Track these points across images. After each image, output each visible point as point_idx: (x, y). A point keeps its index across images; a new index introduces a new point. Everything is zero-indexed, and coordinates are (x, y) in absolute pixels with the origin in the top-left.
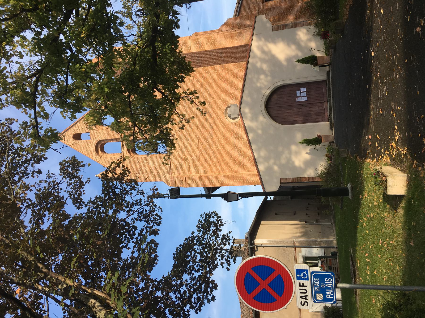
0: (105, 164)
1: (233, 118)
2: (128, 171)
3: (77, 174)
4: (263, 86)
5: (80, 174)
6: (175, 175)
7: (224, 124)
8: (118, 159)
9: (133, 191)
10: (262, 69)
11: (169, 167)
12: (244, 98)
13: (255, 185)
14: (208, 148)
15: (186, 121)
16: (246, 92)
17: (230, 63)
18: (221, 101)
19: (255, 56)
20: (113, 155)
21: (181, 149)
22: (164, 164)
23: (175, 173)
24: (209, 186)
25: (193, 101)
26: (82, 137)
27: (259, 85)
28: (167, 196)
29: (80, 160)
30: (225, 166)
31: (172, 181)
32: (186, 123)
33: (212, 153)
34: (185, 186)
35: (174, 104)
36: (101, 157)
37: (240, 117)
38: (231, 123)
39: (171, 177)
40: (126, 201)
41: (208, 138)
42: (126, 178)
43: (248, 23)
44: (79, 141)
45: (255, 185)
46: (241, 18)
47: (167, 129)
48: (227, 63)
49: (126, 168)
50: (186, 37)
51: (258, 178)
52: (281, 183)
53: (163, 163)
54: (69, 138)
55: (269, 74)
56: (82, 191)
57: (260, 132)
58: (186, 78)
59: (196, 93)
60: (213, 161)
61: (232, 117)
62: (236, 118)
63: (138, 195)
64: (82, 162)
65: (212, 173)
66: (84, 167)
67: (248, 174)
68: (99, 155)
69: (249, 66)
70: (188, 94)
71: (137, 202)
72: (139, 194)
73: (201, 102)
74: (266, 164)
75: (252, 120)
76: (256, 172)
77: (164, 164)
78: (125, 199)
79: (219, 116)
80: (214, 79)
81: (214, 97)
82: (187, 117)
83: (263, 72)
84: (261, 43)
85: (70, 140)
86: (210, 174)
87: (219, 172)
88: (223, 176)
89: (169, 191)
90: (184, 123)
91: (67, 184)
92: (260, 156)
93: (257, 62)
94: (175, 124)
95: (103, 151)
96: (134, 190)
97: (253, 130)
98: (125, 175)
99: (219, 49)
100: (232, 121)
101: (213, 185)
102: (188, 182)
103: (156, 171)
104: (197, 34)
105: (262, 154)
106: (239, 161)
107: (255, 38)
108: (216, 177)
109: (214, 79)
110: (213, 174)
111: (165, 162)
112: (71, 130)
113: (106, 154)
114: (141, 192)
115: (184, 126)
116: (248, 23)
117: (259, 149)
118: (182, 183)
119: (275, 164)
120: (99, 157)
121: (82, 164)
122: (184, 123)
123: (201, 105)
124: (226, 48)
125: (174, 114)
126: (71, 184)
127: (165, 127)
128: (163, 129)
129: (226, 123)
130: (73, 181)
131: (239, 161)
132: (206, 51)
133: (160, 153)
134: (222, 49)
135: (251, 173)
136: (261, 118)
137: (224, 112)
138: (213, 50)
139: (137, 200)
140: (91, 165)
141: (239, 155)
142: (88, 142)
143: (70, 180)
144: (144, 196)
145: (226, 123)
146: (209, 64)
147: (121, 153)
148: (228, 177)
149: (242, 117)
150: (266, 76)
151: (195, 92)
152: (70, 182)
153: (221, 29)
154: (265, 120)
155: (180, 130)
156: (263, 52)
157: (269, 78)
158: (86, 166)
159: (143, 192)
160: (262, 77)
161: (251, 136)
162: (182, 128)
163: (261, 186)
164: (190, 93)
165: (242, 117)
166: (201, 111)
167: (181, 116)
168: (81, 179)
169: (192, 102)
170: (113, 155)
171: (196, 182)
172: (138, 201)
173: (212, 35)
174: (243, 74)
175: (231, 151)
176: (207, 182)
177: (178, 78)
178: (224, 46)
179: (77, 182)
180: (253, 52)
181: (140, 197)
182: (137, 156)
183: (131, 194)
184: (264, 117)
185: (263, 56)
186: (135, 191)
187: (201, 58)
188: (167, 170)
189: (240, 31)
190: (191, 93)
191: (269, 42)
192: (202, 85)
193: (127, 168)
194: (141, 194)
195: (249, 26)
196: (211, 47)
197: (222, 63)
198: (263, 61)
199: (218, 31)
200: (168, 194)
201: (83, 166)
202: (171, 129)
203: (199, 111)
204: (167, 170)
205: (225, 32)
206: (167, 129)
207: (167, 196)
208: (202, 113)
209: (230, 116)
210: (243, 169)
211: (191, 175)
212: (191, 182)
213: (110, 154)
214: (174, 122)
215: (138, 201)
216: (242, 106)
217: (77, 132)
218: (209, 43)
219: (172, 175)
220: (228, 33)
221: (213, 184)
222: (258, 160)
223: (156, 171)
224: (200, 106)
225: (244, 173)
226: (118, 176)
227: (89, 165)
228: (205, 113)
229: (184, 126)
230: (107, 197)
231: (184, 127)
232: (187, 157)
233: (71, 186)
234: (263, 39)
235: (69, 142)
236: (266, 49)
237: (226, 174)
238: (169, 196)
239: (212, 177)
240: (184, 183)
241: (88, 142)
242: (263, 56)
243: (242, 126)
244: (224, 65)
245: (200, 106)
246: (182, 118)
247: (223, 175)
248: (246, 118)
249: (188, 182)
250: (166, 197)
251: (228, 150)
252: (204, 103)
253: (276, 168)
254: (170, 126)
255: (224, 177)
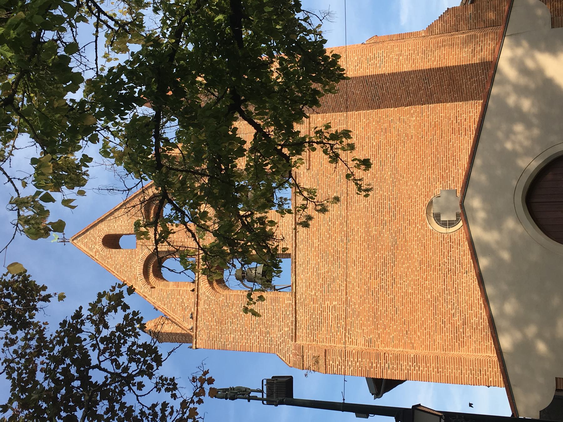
0: (159, 303)
1: (444, 224)
2: (139, 320)
3: (31, 317)
4: (518, 148)
5: (38, 317)
6: (304, 342)
7: (423, 236)
8: (114, 288)
9: (145, 379)
10: (518, 109)
11: (292, 323)
12: (473, 174)
13: (489, 387)
14: (381, 287)
15: (319, 208)
16: (478, 162)
17: (446, 101)
18: (419, 183)
19: (505, 81)
20: (178, 286)
21: (322, 285)
22: (246, 313)
23: (305, 339)
24: (378, 377)
25: (337, 155)
26: (121, 242)
27: (509, 146)
28: (259, 395)
29: (40, 283)
30: (419, 334)
31: (295, 355)
32: (317, 211)
33: (392, 300)
34: (322, 369)
35: (287, 158)
36: (152, 288)
37: (461, 224)
38: (439, 236)
39: (295, 346)
40: (123, 405)
41: (385, 264)
42: (131, 340)
43: (491, 15)
44: (114, 250)
45: (489, 387)
46: (476, 9)
47: (261, 220)
48: (439, 101)
49: (134, 312)
50: (354, 45)
51: (497, 369)
52: (557, 390)
53: (246, 310)
54: (95, 243)
55: (535, 121)
56: (39, 364)
57: (506, 256)
58: (323, 95)
59: (349, 137)
60: (392, 319)
61: (443, 218)
62: (451, 224)
63: (159, 390)
64: (44, 288)
65: (387, 345)
66: (49, 301)
67: (473, 358)
68: (149, 283)
69: (490, 103)
70: (326, 137)
71: (154, 411)
72: (163, 389)
73: (359, 160)
74: (518, 335)
75: (488, 225)
76: (494, 356)
77: (246, 313)
78: (123, 400)
79: (414, 218)
80: (407, 135)
81: (405, 175)
82: (319, 197)
83: (523, 118)
84: (520, 52)
85: (98, 247)
86: (382, 348)
87: (405, 346)
88: (412, 356)
89: (265, 382)
90: (311, 210)
91: (4, 341)
92: (502, 314)
93: (508, 94)
94: (289, 212)
95: (159, 275)
96: (150, 376)
97: (488, 250)
98: (129, 331)
99: (423, 71)
100: (443, 230)
101: (388, 375)
102: (331, 362)
103: (264, 329)
104: (376, 41)
105: (509, 308)
106: (453, 325)
107: (506, 41)
108: (397, 357)
109: (407, 135)
110: (391, 349)
111: (250, 307)
112: (102, 226)
113: (163, 283)
114: (169, 384)
115: (310, 218)
116: (491, 15)
117: (503, 297)
118: (317, 362)
119: (540, 336)
120: (149, 287)
121: (43, 293)
122: (311, 210)
123: (358, 167)
124: (439, 70)
125: (286, 185)
126: (13, 342)
127: (258, 215)
128: (253, 221)
129: (428, 234)
130: (20, 334)
131: (453, 325)
132: (393, 74)
133: (275, 290)
134: (430, 70)
135: (482, 355)
136: (510, 223)
137: (424, 208)
138: (410, 73)
139: (154, 406)
140: (65, 297)
141: (453, 311)
142: (131, 253)
143: (13, 331)
144: (174, 396)
145: (428, 234)
146: (398, 103)
147: (194, 282)
148: (425, 359)
149: (466, 221)
150: (529, 125)
151: (346, 134)
152: (13, 337)
153: (430, 29)
154: (520, 229)
155: (300, 228)
156: (523, 70)
157: (536, 132)
158: (54, 300)
159: (175, 385)
160: (519, 128)
161: (483, 262)
162: (306, 225)
163: (504, 390)
164: (332, 135)
165: (466, 221)
166: (357, 184)
167: (305, 194)
168: (43, 330)
169: (335, 158)
170: (178, 286)
171: (350, 363)
172: (158, 409)
173: (411, 41)
174: (474, 127)
175: (436, 299)
176: (374, 365)
177: (304, 95)
178: (435, 65)
179: (31, 339)
180: (501, 74)
181: (165, 396)
182: (226, 292)
183: (140, 386)
184: (519, 220)
185: (523, 81)
186: (150, 378)
187: (382, 88)
188: (286, 329)
189: (473, 33)
190: (335, 137)
191: (541, 50)
192: (379, 147)
193: (135, 314)
194: (167, 390)
195: (494, 24)
196: (405, 66)
197: (429, 101)
198: (521, 91)
199: (423, 34)
200: (262, 391)
201: (46, 299)
202: (272, 223)
203: (352, 184)
204: (286, 329)
205: (439, 35)
206: (261, 220)
207: (259, 395)
208: (360, 189)
209: (437, 217)
210: (462, 344)
211: (340, 345)
212: (337, 363)
213: (171, 283)
214: (286, 207)
215: (158, 409)
216: (469, 191)
217: (112, 232)
218: (401, 58)
219: (298, 342)
220: (446, 37)
221: (389, 371)
222: (500, 323)
223: (264, 329)
224: (355, 170)
225: (463, 353)
226: (113, 333)
227: (61, 298)
228: (367, 190)
229: (310, 218)
230: (63, 391)
231: (310, 222)
232: (334, 303)
233: (15, 347)
234: (525, 44)
235: (94, 250)
236: (530, 64)
237: (421, 352)
238: (265, 396)
239: (387, 355)
240: (321, 362)
241: (131, 253)
242: (523, 81)
243: (466, 243)
244: (432, 106)
245: (355, 170)
246: (306, 199)
247: (412, 353)
248: (474, 220)
249: (331, 362)
250: (255, 398)
251: (429, 296)
252: (366, 163)
253: (541, 347)
254: (272, 214)
255: (415, 359)
